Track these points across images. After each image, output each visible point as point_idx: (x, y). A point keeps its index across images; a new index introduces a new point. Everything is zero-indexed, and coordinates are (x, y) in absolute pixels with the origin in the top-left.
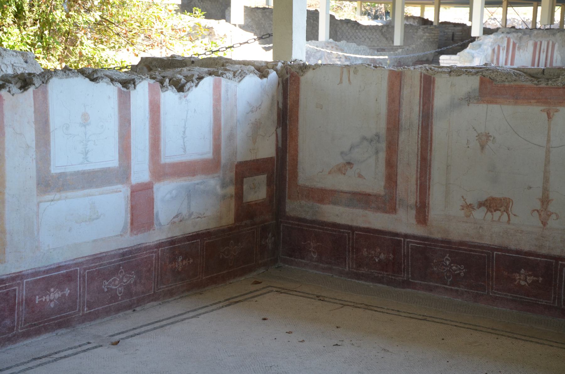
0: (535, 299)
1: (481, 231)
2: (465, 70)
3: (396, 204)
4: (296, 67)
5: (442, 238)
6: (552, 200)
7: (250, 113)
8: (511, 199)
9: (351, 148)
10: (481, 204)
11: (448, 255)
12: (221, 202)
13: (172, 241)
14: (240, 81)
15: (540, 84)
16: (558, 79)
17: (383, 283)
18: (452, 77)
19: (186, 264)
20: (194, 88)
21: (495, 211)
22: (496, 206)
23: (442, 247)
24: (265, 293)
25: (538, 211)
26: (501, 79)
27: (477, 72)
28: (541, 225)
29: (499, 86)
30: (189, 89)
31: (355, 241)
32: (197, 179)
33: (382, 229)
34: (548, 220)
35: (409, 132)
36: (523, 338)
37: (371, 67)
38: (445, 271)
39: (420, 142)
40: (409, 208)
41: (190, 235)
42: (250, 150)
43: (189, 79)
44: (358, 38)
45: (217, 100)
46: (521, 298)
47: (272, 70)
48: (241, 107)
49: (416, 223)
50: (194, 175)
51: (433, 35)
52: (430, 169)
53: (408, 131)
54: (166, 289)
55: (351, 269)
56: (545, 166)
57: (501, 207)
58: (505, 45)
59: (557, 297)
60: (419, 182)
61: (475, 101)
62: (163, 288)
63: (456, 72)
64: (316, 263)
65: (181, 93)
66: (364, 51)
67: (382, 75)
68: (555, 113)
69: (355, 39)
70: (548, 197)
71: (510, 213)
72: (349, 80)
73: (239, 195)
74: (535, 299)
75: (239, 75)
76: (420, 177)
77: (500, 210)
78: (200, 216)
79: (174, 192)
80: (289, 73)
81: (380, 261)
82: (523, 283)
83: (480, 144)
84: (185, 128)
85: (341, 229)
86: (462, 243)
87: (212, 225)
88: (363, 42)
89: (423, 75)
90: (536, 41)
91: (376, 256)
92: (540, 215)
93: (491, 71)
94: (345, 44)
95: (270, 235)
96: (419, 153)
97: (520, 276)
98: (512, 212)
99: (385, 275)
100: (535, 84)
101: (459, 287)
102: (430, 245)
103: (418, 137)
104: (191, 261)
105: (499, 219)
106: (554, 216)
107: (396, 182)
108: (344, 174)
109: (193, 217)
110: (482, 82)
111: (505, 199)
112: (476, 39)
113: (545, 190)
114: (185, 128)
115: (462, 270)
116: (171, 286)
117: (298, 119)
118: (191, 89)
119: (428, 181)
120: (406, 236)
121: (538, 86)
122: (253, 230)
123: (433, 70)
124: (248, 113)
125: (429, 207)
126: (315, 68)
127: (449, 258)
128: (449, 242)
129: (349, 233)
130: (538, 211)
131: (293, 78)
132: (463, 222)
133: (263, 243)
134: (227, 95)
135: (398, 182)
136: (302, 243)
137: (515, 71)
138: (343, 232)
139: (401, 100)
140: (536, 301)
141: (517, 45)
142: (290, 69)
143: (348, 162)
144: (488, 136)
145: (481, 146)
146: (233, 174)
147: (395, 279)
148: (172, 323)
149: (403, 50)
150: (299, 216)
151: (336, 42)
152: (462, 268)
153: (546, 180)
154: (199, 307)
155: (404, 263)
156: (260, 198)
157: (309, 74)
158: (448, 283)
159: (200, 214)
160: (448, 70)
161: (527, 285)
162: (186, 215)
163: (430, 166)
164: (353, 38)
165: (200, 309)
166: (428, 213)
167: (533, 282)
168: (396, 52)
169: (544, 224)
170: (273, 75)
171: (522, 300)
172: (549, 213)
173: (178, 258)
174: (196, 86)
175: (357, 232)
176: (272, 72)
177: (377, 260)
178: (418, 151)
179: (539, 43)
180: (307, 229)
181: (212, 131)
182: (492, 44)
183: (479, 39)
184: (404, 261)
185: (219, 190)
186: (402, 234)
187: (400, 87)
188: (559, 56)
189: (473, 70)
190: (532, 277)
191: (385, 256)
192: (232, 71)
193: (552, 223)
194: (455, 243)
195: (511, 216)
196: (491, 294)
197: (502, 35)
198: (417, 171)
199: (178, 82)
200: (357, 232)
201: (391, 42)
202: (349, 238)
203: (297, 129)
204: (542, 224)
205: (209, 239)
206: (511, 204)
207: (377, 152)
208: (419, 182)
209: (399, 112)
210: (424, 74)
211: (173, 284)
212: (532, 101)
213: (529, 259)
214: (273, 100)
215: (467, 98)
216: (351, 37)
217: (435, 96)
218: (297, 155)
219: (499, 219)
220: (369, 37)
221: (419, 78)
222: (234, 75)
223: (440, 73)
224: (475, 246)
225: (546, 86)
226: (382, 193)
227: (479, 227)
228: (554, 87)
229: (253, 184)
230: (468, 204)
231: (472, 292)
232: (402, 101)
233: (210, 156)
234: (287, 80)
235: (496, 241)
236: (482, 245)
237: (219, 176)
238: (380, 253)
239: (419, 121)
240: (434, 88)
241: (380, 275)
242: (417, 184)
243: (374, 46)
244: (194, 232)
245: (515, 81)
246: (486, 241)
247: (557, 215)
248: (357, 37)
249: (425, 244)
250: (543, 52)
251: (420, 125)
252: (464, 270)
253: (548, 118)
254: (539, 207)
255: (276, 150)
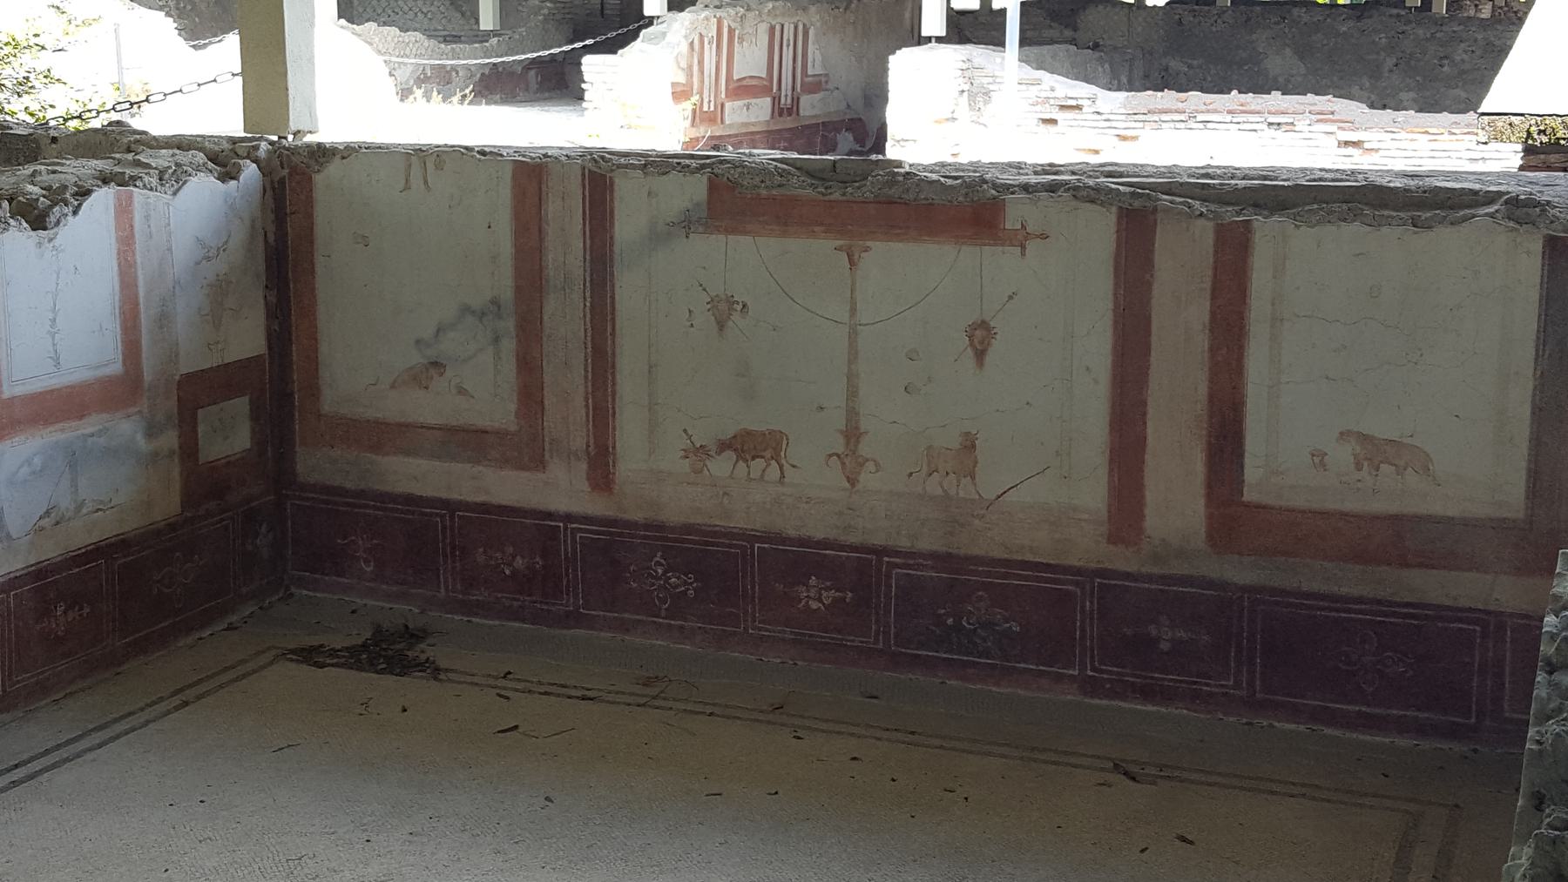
0: (840, 637)
1: (726, 501)
2: (675, 160)
3: (544, 450)
4: (301, 151)
5: (646, 519)
6: (866, 433)
7: (204, 262)
8: (784, 434)
9: (438, 331)
10: (723, 446)
11: (659, 554)
12: (147, 468)
13: (40, 571)
14: (175, 194)
15: (831, 194)
16: (864, 182)
17: (524, 621)
18: (649, 178)
19: (74, 618)
20: (70, 218)
21: (753, 458)
22: (755, 448)
23: (645, 537)
24: (263, 668)
25: (838, 456)
26: (750, 181)
27: (703, 166)
28: (847, 485)
29: (749, 196)
30: (58, 223)
31: (456, 531)
32: (90, 425)
33: (516, 505)
34: (859, 473)
35: (565, 294)
36: (824, 726)
37: (473, 153)
38: (655, 587)
39: (588, 316)
40: (572, 458)
41: (80, 552)
42: (209, 344)
43: (56, 195)
44: (401, 13)
45: (126, 241)
46: (811, 636)
47: (248, 161)
48: (183, 250)
49: (589, 490)
50: (81, 417)
51: (562, 5)
52: (613, 374)
53: (563, 292)
54: (32, 680)
55: (451, 594)
56: (850, 362)
57: (765, 450)
58: (714, 33)
59: (882, 629)
60: (590, 401)
61: (701, 229)
62: (23, 680)
63: (657, 166)
64: (372, 585)
65: (41, 232)
66: (417, 45)
67: (498, 172)
68: (863, 255)
69: (392, 14)
70: (857, 428)
71: (783, 462)
72: (426, 182)
73: (189, 450)
74: (840, 637)
75: (174, 178)
76: (593, 392)
77: (762, 457)
78: (101, 507)
79: (37, 461)
80: (285, 166)
81: (514, 573)
82: (814, 605)
83: (716, 318)
84: (54, 310)
85: (426, 508)
86: (689, 529)
87: (132, 524)
88: (410, 20)
89: (587, 171)
90: (773, 23)
91: (504, 564)
92: (843, 464)
93: (729, 165)
94: (375, 30)
95: (264, 529)
96: (589, 338)
97: (808, 591)
98: (787, 462)
99: (527, 603)
100: (818, 192)
101: (685, 620)
102: (621, 534)
103: (585, 305)
104: (87, 610)
105: (762, 476)
106: (870, 466)
107: (542, 402)
108: (426, 388)
109: (84, 511)
110: (713, 187)
111: (771, 432)
112: (655, 22)
113: (852, 414)
114: (54, 310)
115: (691, 583)
116: (43, 672)
117: (313, 268)
118: (63, 222)
119: (610, 399)
120: (568, 518)
121: (826, 198)
122: (224, 523)
123: (606, 162)
124: (198, 263)
125: (614, 454)
126: (345, 155)
127: (662, 561)
128: (660, 527)
129: (442, 516)
130: (838, 456)
131: (297, 177)
132: (689, 484)
133: (250, 548)
134: (149, 226)
135: (546, 402)
136: (339, 541)
137: (779, 165)
138: (431, 515)
139: (544, 225)
140: (842, 640)
141: (737, 32)
142: (288, 155)
143: (432, 361)
144: (731, 302)
145: (718, 323)
146: (173, 403)
147: (548, 611)
148: (54, 766)
149: (501, 39)
150: (328, 483)
151: (355, 26)
152: (690, 581)
153: (852, 393)
154: (116, 716)
155: (567, 575)
156: (237, 450)
157: (334, 169)
158: (663, 613)
159: (101, 502)
160: (640, 160)
161: (822, 608)
162: (67, 509)
163: (613, 366)
164: (390, 12)
165: (116, 721)
166: (614, 466)
167: (835, 600)
168: (487, 44)
169: (852, 481)
170: (250, 171)
171: (815, 639)
172: (860, 460)
173: (56, 607)
174: (75, 213)
175: (461, 514)
176: (249, 166)
177: (507, 572)
178: (586, 336)
179: (778, 28)
180: (349, 509)
181: (117, 311)
182: (688, 31)
183: (660, 20)
184: (567, 570)
185: (141, 442)
186: (560, 513)
187: (540, 199)
188: (817, 52)
189: (693, 161)
190: (833, 591)
191: (525, 561)
192: (156, 168)
193: (867, 479)
194: (673, 529)
195: (786, 466)
196: (750, 631)
197: (706, 13)
198: (586, 377)
199: (31, 205)
200: (461, 514)
201: (473, 21)
202: (444, 528)
203: (313, 289)
204: (849, 482)
205: (125, 557)
206: (785, 442)
207: (496, 340)
208: (590, 401)
209: (541, 251)
210: (589, 171)
211: (46, 668)
212: (817, 229)
213: (825, 555)
214: (253, 227)
215: (684, 221)
216: (384, 11)
217: (616, 217)
218: (317, 349)
219: (762, 476)
220: (425, 10)
221: (580, 178)
222: (161, 179)
223: (623, 168)
224: (715, 534)
225: (841, 198)
226: (513, 428)
227: (721, 493)
228: (858, 200)
229: (220, 420)
230: (698, 446)
231: (712, 629)
232: (546, 227)
233: (116, 368)
234: (282, 181)
235: (758, 523)
236: (729, 530)
237: (140, 412)
238: (514, 557)
239: (585, 271)
240: (612, 200)
241: (515, 603)
242: (587, 406)
243: (436, 30)
244: (90, 545)
245: (779, 186)
246: (739, 522)
247: (877, 464)
248: (396, 10)
249: (610, 534)
250: (788, 46)
251: (588, 279)
252: (695, 585)
253: (850, 264)
254: (840, 449)
255: (268, 338)
